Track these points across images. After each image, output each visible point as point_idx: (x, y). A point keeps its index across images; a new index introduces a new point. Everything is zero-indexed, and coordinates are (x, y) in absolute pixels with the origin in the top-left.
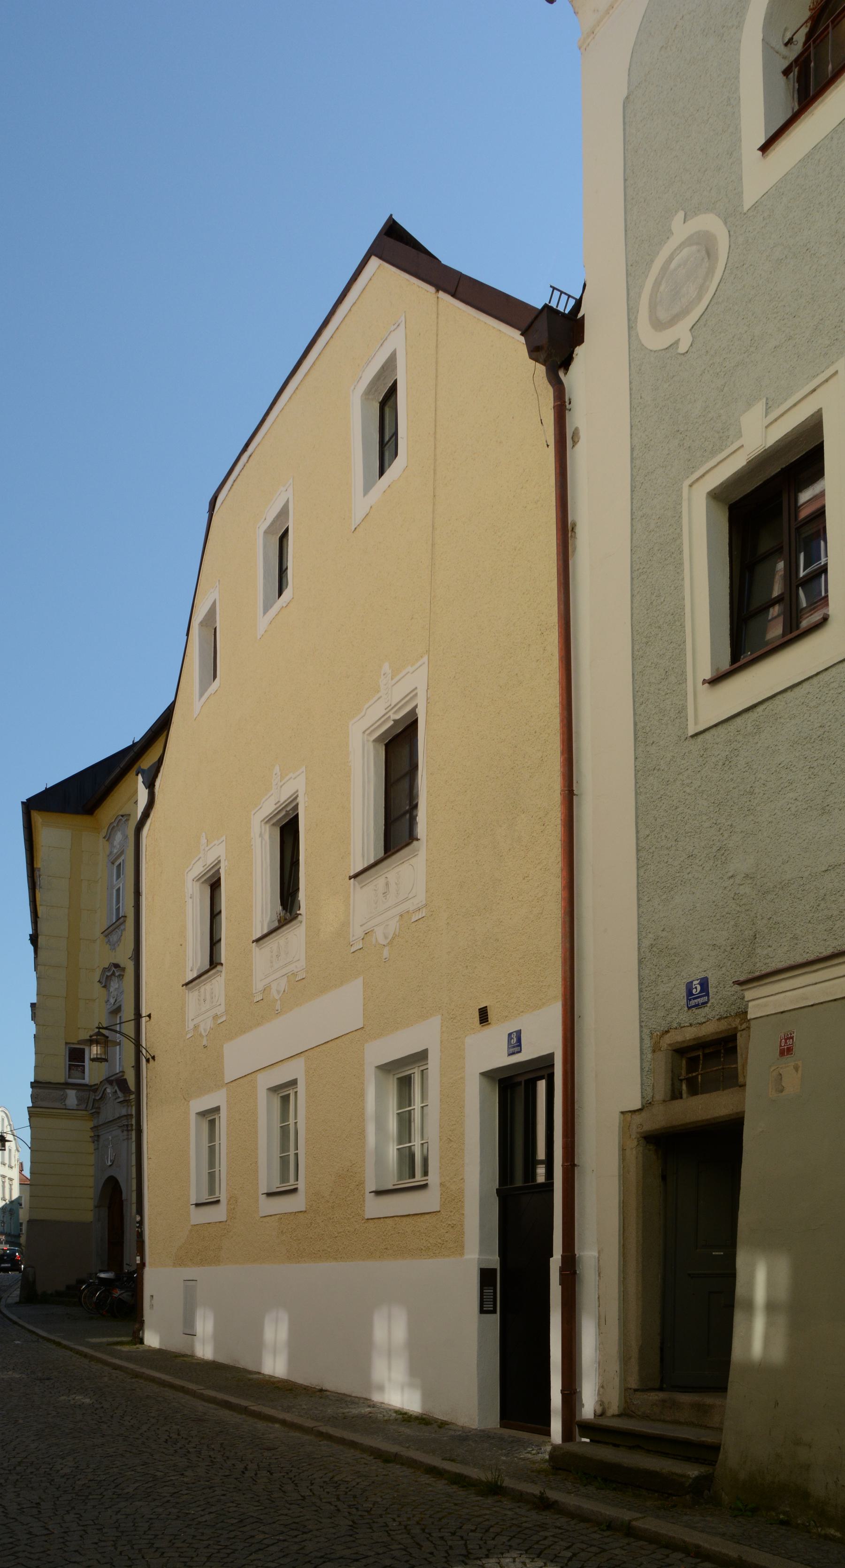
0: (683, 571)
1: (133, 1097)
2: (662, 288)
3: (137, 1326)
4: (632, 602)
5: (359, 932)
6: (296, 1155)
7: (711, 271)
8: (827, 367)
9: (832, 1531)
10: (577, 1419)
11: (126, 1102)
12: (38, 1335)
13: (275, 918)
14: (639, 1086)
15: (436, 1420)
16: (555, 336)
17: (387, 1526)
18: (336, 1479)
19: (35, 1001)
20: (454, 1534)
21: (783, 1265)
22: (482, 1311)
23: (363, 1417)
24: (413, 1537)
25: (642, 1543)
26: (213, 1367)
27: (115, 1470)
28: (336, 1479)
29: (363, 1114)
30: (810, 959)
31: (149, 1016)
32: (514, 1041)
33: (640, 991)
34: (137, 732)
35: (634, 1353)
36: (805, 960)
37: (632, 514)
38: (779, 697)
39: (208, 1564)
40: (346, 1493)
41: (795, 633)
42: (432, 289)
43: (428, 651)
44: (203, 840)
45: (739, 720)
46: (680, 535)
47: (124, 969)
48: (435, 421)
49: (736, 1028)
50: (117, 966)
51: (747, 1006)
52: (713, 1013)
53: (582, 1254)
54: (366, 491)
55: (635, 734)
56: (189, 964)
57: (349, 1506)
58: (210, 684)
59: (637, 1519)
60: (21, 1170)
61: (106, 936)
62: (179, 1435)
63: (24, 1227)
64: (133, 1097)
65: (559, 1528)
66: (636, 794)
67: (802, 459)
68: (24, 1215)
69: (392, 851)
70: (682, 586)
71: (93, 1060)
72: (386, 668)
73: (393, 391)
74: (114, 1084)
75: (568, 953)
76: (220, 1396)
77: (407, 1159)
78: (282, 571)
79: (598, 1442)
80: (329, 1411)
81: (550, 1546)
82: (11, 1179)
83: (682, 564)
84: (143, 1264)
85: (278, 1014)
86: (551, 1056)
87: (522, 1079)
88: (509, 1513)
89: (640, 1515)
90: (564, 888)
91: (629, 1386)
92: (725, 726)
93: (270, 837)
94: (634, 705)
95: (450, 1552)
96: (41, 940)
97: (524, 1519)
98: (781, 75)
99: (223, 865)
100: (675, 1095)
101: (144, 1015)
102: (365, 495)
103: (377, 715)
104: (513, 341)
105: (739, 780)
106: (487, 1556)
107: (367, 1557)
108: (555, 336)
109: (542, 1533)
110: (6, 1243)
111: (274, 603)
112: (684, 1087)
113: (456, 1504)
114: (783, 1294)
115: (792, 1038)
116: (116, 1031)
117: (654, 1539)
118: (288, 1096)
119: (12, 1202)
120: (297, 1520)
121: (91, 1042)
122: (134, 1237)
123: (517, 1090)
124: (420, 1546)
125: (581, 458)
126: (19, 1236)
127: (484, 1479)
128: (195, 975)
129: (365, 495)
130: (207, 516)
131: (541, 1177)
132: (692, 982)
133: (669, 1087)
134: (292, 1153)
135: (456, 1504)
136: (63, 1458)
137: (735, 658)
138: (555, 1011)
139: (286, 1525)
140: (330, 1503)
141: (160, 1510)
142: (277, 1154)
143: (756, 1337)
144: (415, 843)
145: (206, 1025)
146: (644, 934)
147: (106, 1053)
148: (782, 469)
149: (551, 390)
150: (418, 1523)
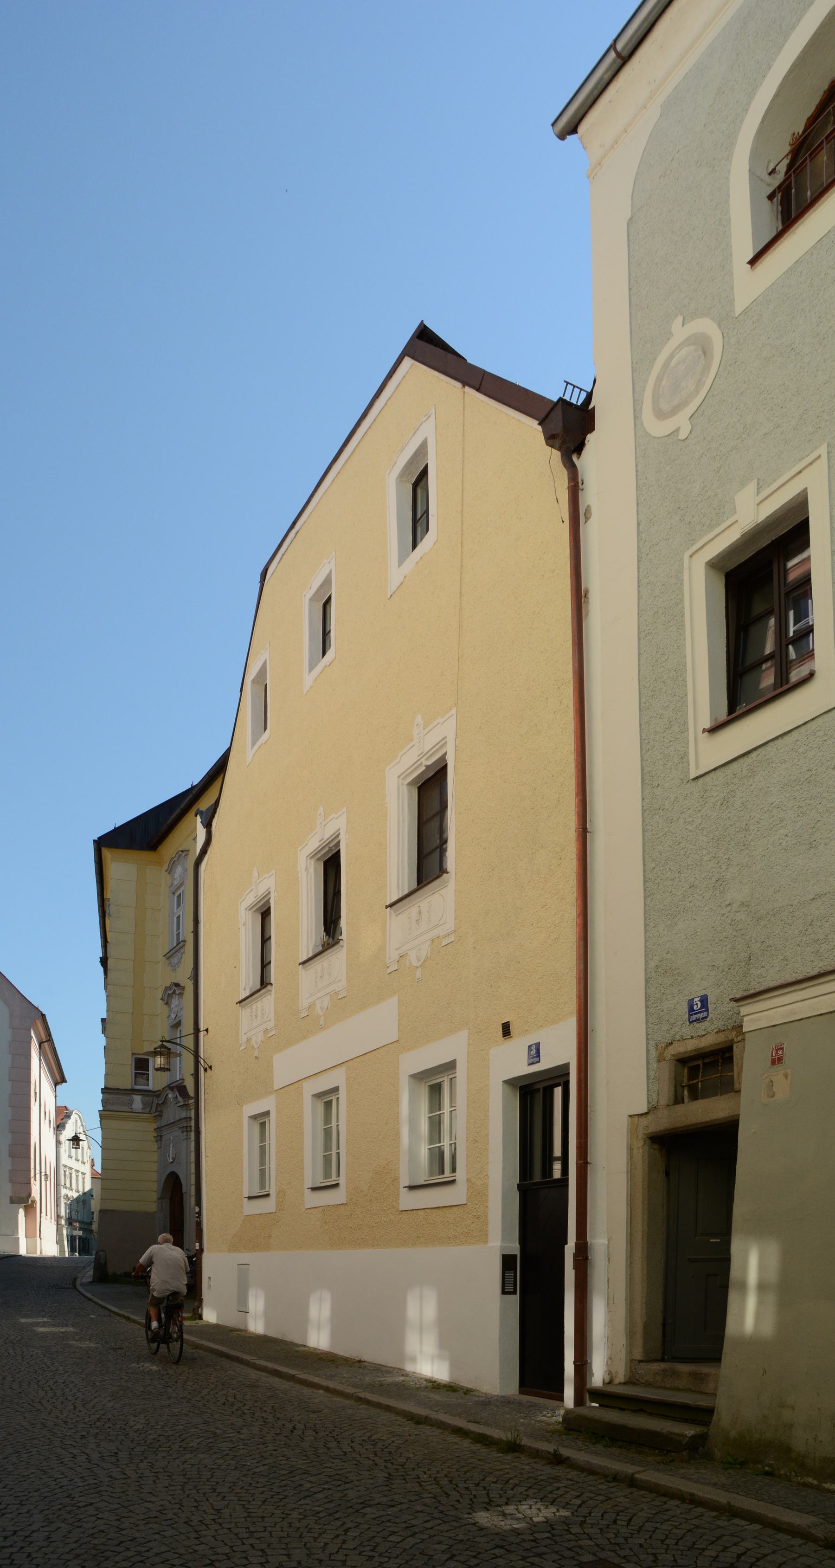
0: (684, 632)
1: (192, 1101)
2: (664, 383)
3: (196, 1304)
4: (639, 660)
5: (395, 956)
6: (338, 1153)
7: (707, 368)
8: (812, 452)
9: (810, 1480)
10: (588, 1386)
11: (186, 1106)
12: (109, 1310)
13: (320, 943)
14: (646, 1093)
15: (462, 1388)
16: (569, 425)
17: (418, 1478)
18: (373, 1438)
19: (105, 1016)
20: (477, 1485)
21: (774, 1250)
22: (504, 1292)
23: (396, 1385)
24: (441, 1488)
25: (642, 1492)
26: (264, 1341)
27: (181, 1427)
28: (373, 1438)
29: (398, 1117)
30: (799, 978)
31: (207, 1030)
32: (534, 1052)
33: (647, 1007)
34: (196, 777)
35: (639, 1329)
36: (794, 980)
37: (639, 581)
38: (771, 744)
39: (263, 1507)
40: (383, 1450)
41: (784, 687)
42: (459, 385)
43: (456, 704)
44: (255, 874)
45: (735, 765)
46: (682, 601)
47: (183, 988)
48: (462, 499)
49: (732, 1040)
50: (177, 985)
51: (742, 1021)
52: (712, 1027)
53: (593, 1241)
54: (401, 562)
55: (642, 778)
56: (243, 984)
57: (386, 1461)
58: (261, 735)
59: (639, 1472)
60: (93, 1166)
61: (168, 958)
62: (235, 1398)
63: (96, 1216)
64: (192, 1101)
65: (571, 1480)
66: (644, 831)
67: (790, 533)
68: (95, 1205)
69: (425, 883)
70: (684, 645)
71: (157, 1070)
72: (419, 719)
73: (424, 473)
74: (175, 1090)
75: (582, 974)
76: (270, 1365)
77: (438, 1158)
78: (326, 634)
79: (607, 1406)
80: (367, 1379)
81: (562, 1496)
82: (84, 1174)
83: (684, 626)
84: (201, 1250)
85: (322, 1028)
86: (566, 1066)
87: (541, 1086)
88: (527, 1467)
89: (642, 1469)
90: (578, 916)
91: (634, 1358)
92: (723, 769)
93: (315, 870)
94: (641, 752)
95: (474, 1500)
96: (110, 962)
97: (539, 1473)
98: (766, 199)
99: (272, 896)
100: (678, 1100)
101: (202, 1029)
102: (399, 566)
103: (411, 761)
104: (530, 429)
105: (736, 818)
106: (507, 1504)
107: (401, 1503)
108: (569, 425)
109: (555, 1485)
110: (80, 1229)
111: (319, 661)
112: (686, 1093)
113: (479, 1460)
114: (773, 1276)
115: (782, 1049)
116: (176, 1044)
117: (655, 1490)
118: (331, 1101)
119: (84, 1194)
120: (339, 1472)
121: (155, 1053)
122: (194, 1226)
123: (535, 1096)
124: (448, 1495)
125: (591, 531)
126: (91, 1224)
127: (504, 1439)
128: (248, 994)
129: (399, 566)
130: (258, 585)
131: (557, 1174)
132: (693, 999)
133: (672, 1093)
134: (334, 1152)
135: (479, 1460)
136: (135, 1416)
137: (731, 709)
138: (571, 1026)
139: (330, 1477)
140: (368, 1458)
141: (220, 1461)
142: (320, 1152)
143: (749, 1314)
144: (445, 875)
145: (258, 1038)
146: (650, 956)
147: (169, 1063)
148: (773, 541)
149: (566, 472)
150: (446, 1476)
